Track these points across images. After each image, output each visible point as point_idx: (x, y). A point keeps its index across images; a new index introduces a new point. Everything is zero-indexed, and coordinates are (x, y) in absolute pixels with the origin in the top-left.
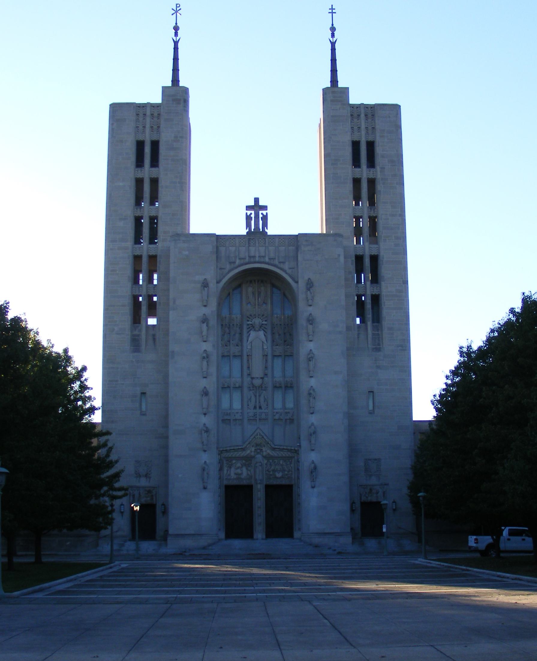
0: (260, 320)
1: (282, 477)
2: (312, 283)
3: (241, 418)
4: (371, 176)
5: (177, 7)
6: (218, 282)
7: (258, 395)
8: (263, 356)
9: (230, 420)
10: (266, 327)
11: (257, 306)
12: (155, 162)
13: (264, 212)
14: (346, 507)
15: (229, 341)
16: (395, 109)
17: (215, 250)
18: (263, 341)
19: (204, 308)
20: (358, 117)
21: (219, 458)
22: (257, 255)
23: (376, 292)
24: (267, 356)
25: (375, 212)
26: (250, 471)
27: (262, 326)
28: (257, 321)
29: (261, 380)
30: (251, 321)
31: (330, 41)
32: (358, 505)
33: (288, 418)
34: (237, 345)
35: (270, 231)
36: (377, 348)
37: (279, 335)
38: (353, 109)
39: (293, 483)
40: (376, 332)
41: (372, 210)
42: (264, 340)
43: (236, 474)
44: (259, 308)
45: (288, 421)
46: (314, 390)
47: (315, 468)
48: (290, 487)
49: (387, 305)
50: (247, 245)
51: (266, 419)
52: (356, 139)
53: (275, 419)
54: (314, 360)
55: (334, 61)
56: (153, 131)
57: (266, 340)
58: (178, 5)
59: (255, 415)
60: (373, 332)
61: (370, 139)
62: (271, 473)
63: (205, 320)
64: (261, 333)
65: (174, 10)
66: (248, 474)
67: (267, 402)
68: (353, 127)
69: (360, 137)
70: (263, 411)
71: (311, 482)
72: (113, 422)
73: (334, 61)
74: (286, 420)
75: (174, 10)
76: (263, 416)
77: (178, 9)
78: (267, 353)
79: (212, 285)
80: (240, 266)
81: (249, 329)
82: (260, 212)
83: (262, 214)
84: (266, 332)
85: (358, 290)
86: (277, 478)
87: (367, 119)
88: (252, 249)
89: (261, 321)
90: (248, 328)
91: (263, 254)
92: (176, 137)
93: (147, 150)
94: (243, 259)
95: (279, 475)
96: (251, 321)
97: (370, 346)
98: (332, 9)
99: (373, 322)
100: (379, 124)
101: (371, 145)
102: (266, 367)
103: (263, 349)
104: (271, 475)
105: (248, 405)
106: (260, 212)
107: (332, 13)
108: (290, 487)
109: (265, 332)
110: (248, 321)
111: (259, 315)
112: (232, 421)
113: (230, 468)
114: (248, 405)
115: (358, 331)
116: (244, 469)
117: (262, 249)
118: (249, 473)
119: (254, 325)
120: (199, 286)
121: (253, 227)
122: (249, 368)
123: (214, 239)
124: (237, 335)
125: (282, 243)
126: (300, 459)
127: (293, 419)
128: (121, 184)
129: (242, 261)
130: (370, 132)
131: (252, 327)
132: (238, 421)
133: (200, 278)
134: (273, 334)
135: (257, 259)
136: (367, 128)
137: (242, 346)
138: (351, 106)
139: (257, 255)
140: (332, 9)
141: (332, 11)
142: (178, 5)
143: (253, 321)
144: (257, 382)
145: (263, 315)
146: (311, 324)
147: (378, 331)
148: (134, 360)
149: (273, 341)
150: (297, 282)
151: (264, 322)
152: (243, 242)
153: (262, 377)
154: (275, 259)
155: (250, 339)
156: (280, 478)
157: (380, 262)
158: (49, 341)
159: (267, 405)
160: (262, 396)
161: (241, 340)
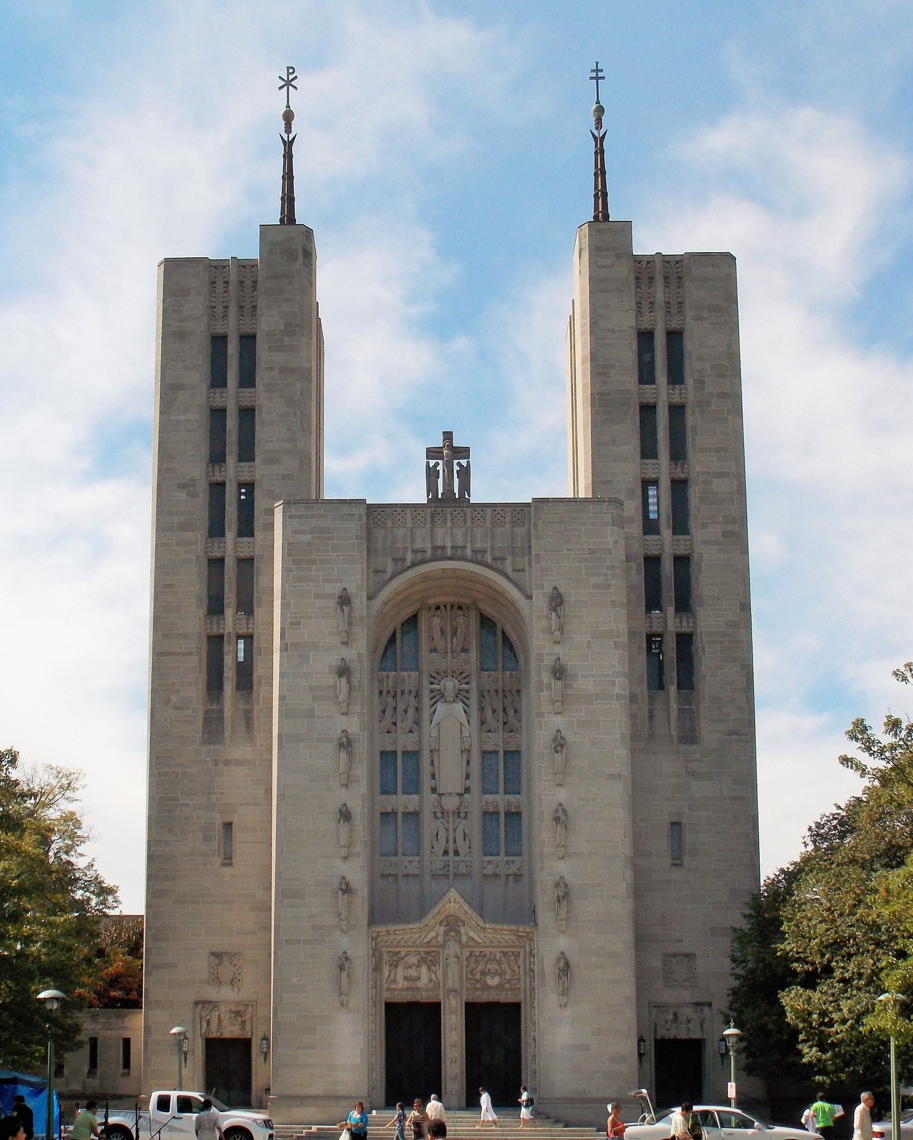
0: (456, 681)
1: (500, 987)
2: (560, 595)
3: (418, 872)
4: (676, 399)
5: (289, 73)
6: (370, 598)
8: (462, 751)
10: (467, 695)
11: (449, 655)
13: (464, 462)
14: (629, 1047)
15: (395, 724)
16: (726, 260)
17: (365, 534)
18: (462, 722)
19: (344, 647)
20: (650, 283)
21: (373, 947)
22: (449, 545)
23: (685, 628)
25: (686, 470)
26: (436, 973)
27: (461, 692)
30: (439, 683)
32: (650, 1047)
33: (510, 872)
34: (411, 732)
35: (476, 497)
36: (689, 737)
37: (494, 711)
38: (639, 265)
39: (522, 997)
41: (679, 466)
43: (406, 978)
44: (454, 658)
45: (511, 878)
46: (564, 811)
47: (567, 964)
48: (515, 1008)
50: (429, 525)
52: (646, 325)
53: (485, 875)
55: (601, 172)
56: (244, 314)
57: (468, 722)
58: (291, 70)
59: (446, 866)
60: (680, 706)
61: (674, 325)
62: (478, 977)
63: (344, 671)
64: (459, 707)
65: (288, 89)
66: (431, 980)
67: (470, 841)
68: (640, 303)
69: (652, 322)
70: (462, 858)
73: (601, 172)
74: (508, 875)
75: (288, 89)
76: (462, 869)
77: (291, 77)
79: (360, 603)
80: (414, 565)
81: (434, 700)
82: (455, 462)
83: (459, 464)
84: (468, 706)
85: (651, 618)
86: (490, 987)
87: (668, 285)
88: (440, 532)
89: (458, 683)
91: (460, 543)
92: (287, 325)
95: (494, 981)
96: (439, 683)
97: (674, 733)
98: (597, 71)
100: (694, 293)
101: (675, 337)
102: (468, 776)
104: (477, 981)
105: (433, 848)
107: (597, 78)
108: (515, 1008)
109: (465, 707)
110: (432, 683)
111: (453, 672)
112: (400, 878)
113: (396, 966)
114: (433, 848)
116: (424, 970)
117: (459, 533)
118: (433, 976)
119: (443, 691)
120: (332, 603)
122: (433, 777)
123: (362, 511)
124: (411, 712)
125: (499, 519)
126: (535, 951)
128: (182, 417)
129: (419, 557)
130: (674, 310)
131: (438, 696)
133: (337, 589)
135: (449, 552)
136: (669, 303)
138: (636, 259)
139: (449, 545)
140: (597, 71)
141: (597, 75)
142: (291, 70)
143: (441, 683)
144: (451, 803)
146: (559, 679)
147: (691, 705)
148: (208, 759)
149: (483, 723)
150: (529, 597)
152: (421, 524)
153: (460, 792)
155: (436, 719)
156: (497, 987)
159: (470, 848)
160: (460, 832)
161: (417, 723)
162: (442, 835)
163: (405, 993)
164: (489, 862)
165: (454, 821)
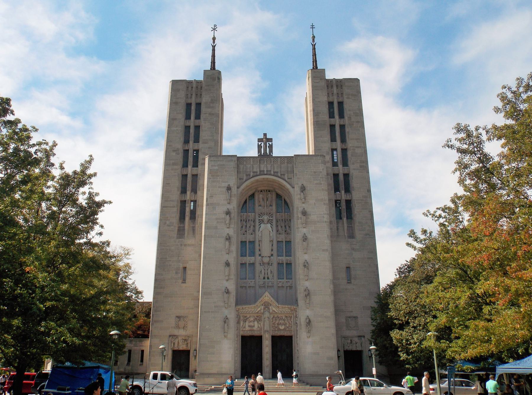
1: (284, 329)
3: (254, 285)
4: (342, 123)
5: (214, 27)
6: (238, 188)
7: (266, 268)
8: (270, 241)
9: (246, 287)
11: (266, 207)
12: (198, 117)
13: (270, 143)
15: (246, 231)
17: (236, 166)
24: (273, 241)
26: (260, 324)
28: (266, 218)
29: (269, 258)
31: (312, 44)
32: (342, 354)
33: (288, 285)
34: (252, 234)
35: (275, 154)
36: (352, 236)
37: (281, 227)
40: (350, 225)
42: (271, 230)
43: (249, 326)
45: (288, 288)
46: (307, 263)
47: (310, 321)
48: (291, 337)
49: (357, 209)
50: (258, 164)
51: (273, 286)
53: (278, 287)
54: (307, 241)
55: (314, 55)
58: (215, 26)
59: (264, 283)
61: (340, 100)
62: (276, 326)
63: (228, 213)
64: (269, 225)
66: (258, 327)
71: (307, 333)
72: (161, 288)
73: (314, 55)
74: (287, 287)
76: (270, 284)
77: (215, 28)
78: (273, 239)
79: (234, 190)
80: (253, 177)
83: (269, 144)
84: (272, 225)
86: (281, 330)
90: (259, 222)
93: (193, 108)
94: (255, 172)
95: (282, 327)
98: (313, 26)
99: (347, 218)
100: (346, 90)
102: (272, 250)
103: (270, 236)
106: (268, 143)
107: (313, 28)
108: (291, 337)
110: (259, 217)
112: (247, 288)
113: (245, 322)
115: (337, 225)
116: (256, 323)
117: (269, 166)
118: (260, 326)
121: (262, 152)
122: (260, 250)
123: (236, 159)
124: (252, 227)
127: (292, 287)
129: (255, 174)
131: (261, 222)
132: (251, 288)
133: (226, 185)
134: (277, 226)
135: (265, 173)
137: (255, 234)
140: (313, 26)
141: (313, 27)
142: (215, 26)
144: (266, 260)
145: (270, 214)
149: (277, 231)
150: (294, 188)
151: (271, 218)
154: (278, 172)
156: (283, 330)
157: (350, 178)
158: (103, 210)
160: (269, 270)
161: (254, 231)
162: (263, 271)
163: (249, 332)
164: (280, 282)
165: (267, 267)
